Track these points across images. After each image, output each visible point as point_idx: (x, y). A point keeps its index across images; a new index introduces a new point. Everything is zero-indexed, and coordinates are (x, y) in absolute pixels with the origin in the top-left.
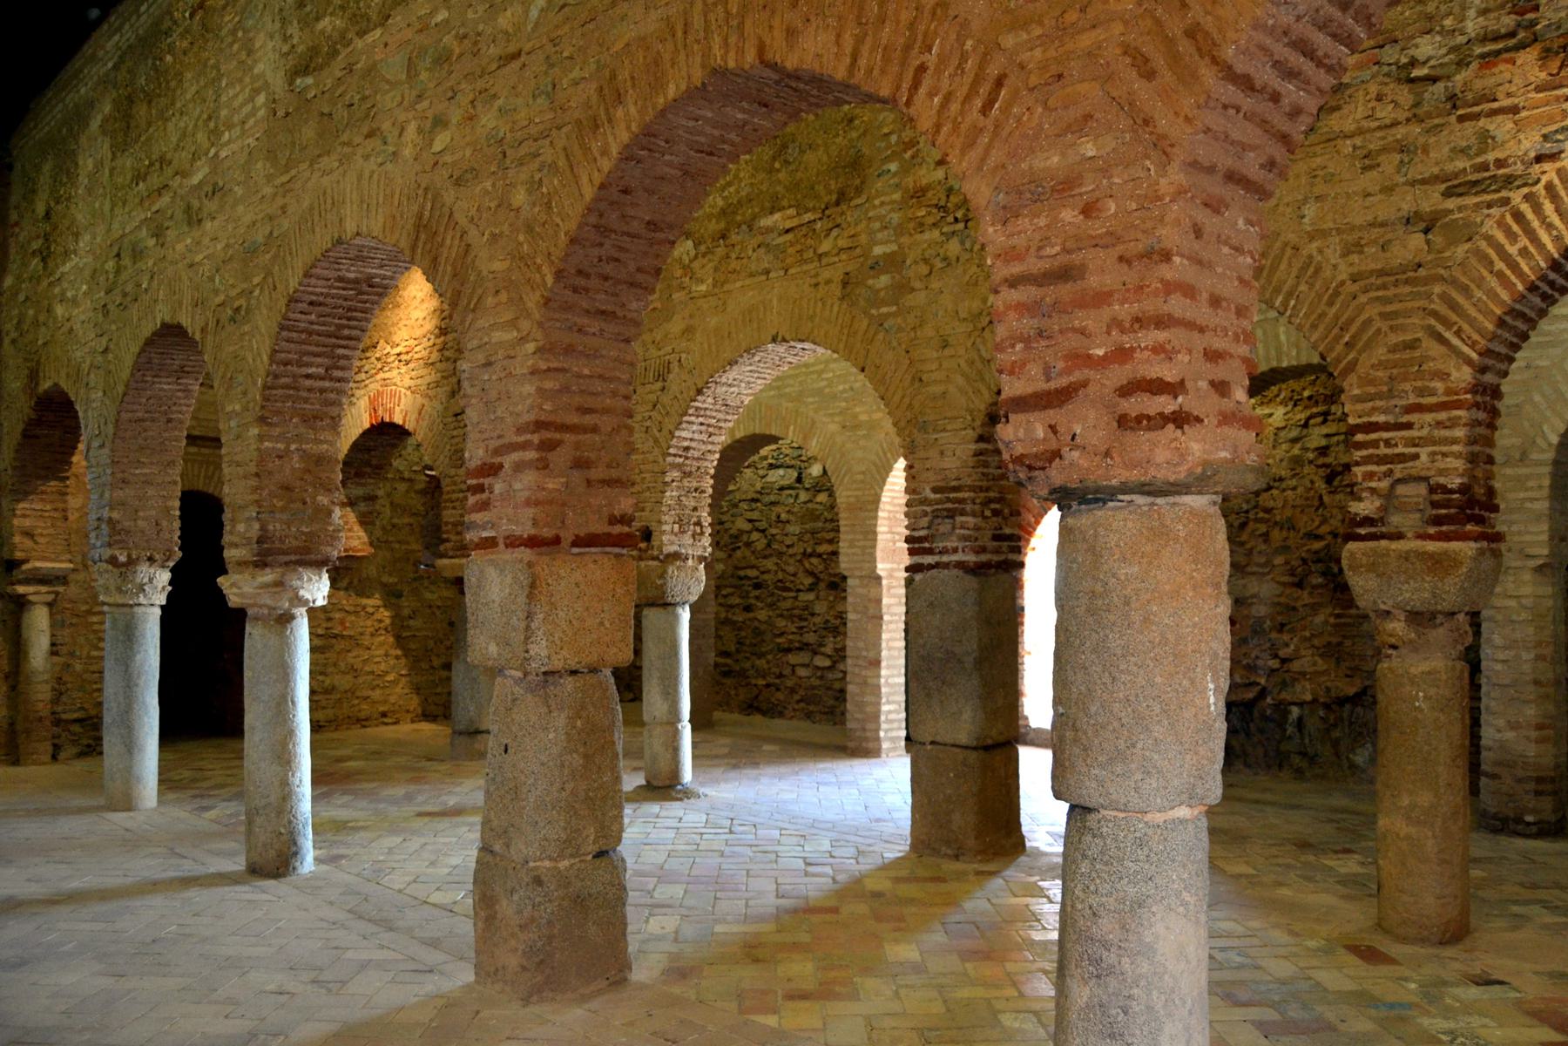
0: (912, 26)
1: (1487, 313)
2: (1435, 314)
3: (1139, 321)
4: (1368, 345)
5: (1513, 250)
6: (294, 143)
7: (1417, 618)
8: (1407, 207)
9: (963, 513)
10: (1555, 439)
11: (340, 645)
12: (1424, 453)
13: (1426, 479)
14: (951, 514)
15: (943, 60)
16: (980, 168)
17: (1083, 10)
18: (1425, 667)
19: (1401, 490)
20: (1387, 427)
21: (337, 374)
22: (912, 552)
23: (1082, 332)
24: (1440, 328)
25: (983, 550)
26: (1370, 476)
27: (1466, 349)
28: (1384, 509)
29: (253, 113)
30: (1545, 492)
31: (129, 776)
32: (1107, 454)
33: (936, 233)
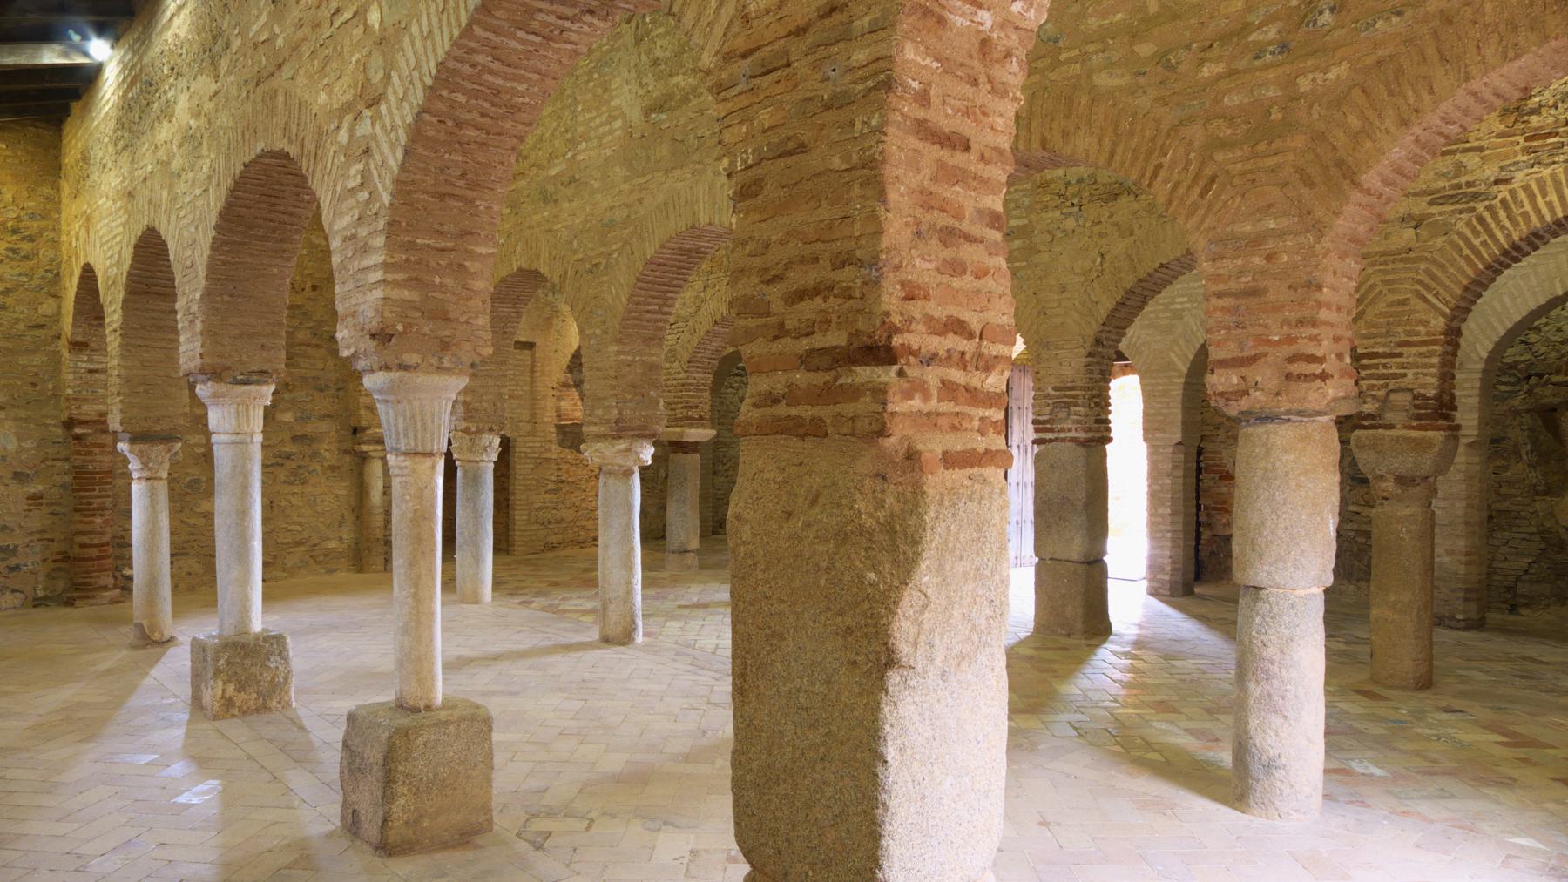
0: (1153, 139)
1: (1458, 283)
2: (1420, 282)
3: (1301, 322)
4: (1373, 302)
5: (1476, 242)
6: (648, 158)
7: (1401, 480)
8: (1403, 210)
9: (1076, 405)
10: (1485, 355)
11: (566, 488)
12: (1410, 373)
13: (1411, 390)
14: (1067, 405)
15: (1173, 162)
16: (1198, 228)
17: (1269, 144)
18: (1408, 511)
19: (1393, 397)
20: (1385, 355)
21: (666, 309)
22: (1037, 430)
23: (1266, 326)
24: (1424, 292)
25: (1090, 430)
26: (1372, 387)
27: (1441, 306)
28: (1382, 410)
29: (611, 132)
30: (1477, 392)
31: (477, 579)
32: (1278, 394)
33: (1058, 213)
